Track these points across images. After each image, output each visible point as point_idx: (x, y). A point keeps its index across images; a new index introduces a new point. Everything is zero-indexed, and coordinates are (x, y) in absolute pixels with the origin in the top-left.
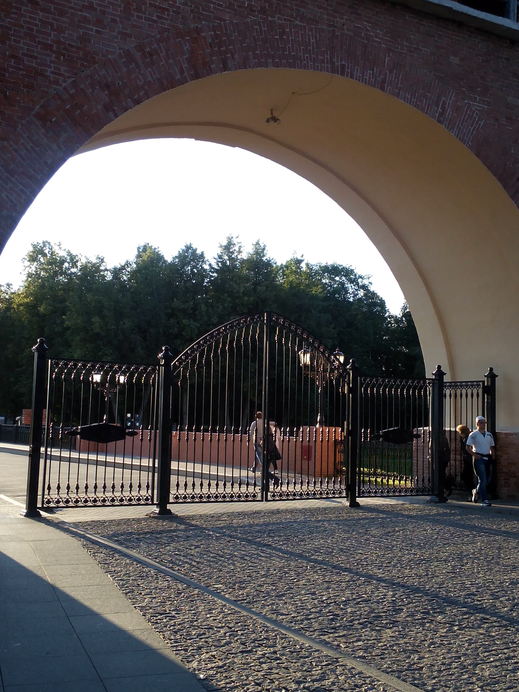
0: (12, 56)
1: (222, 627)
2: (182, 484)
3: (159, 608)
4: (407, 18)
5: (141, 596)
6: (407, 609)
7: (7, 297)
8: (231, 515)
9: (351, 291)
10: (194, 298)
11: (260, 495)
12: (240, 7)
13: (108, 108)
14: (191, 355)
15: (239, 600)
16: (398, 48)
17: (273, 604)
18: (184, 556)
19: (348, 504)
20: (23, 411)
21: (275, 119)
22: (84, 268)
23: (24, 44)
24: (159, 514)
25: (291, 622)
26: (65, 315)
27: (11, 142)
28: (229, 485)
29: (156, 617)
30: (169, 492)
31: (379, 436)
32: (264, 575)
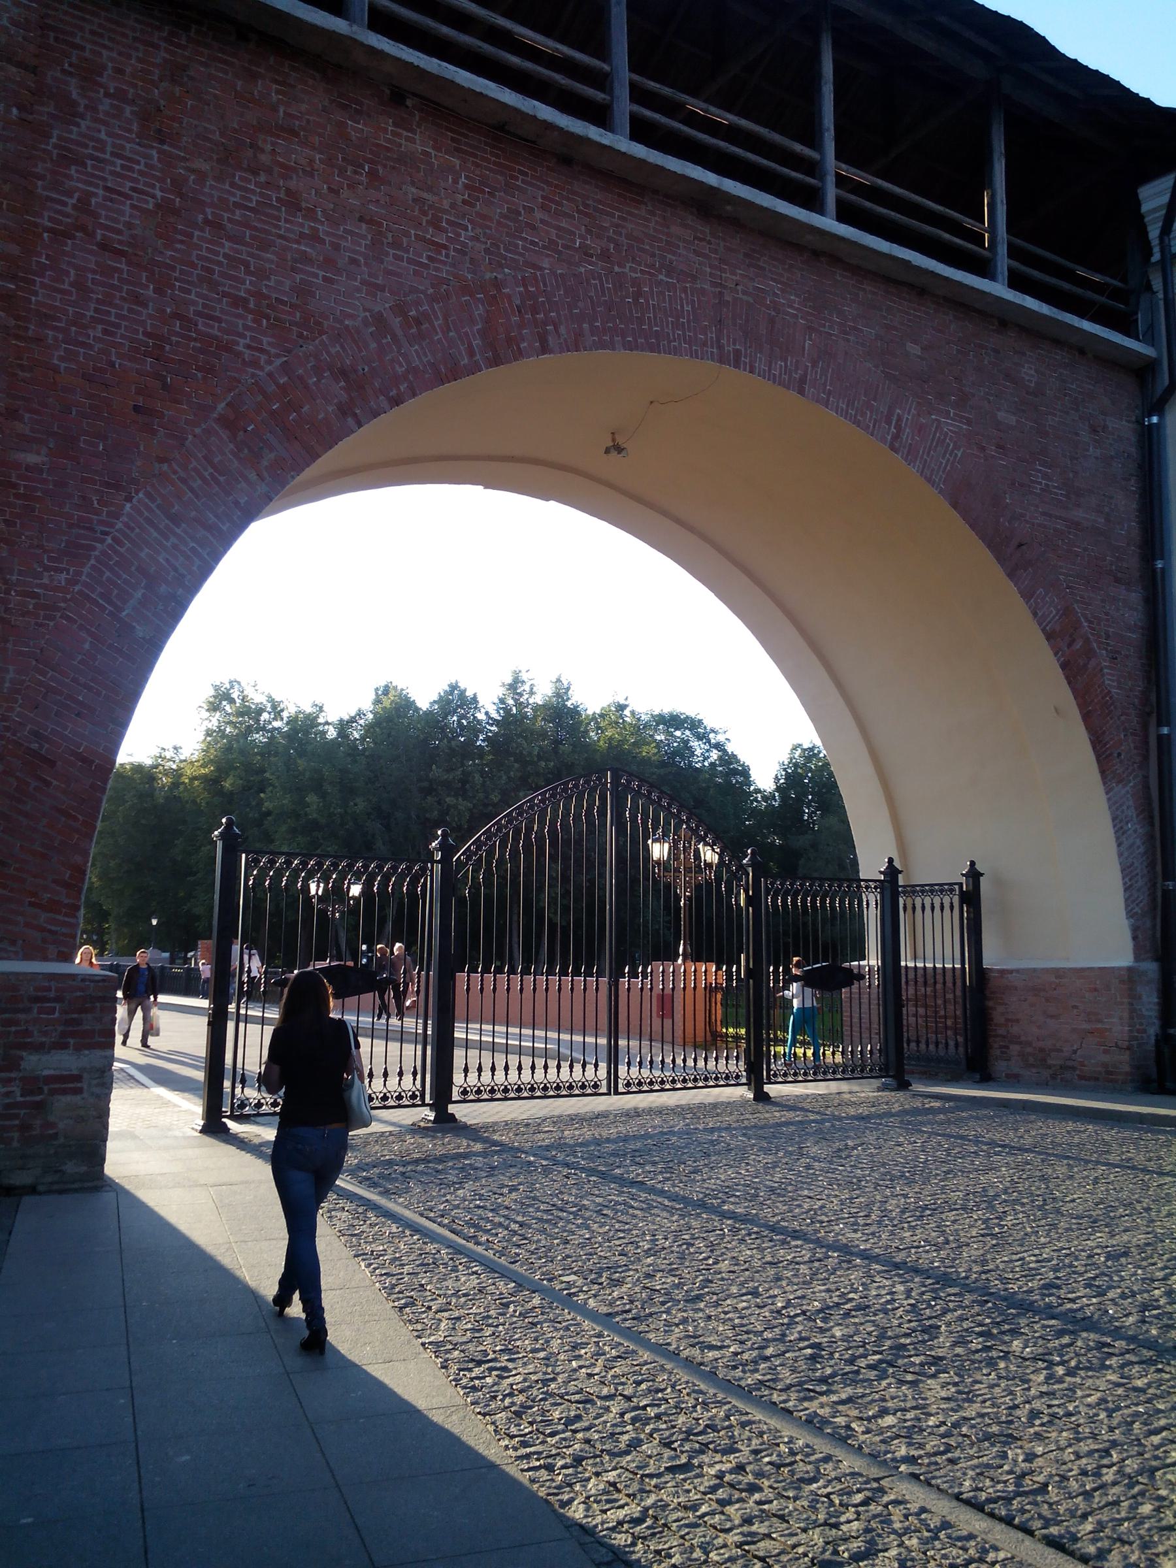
0: (176, 316)
2: (473, 1065)
5: (431, 1315)
6: (948, 1324)
7: (174, 767)
8: (559, 1121)
9: (698, 752)
10: (463, 765)
11: (604, 1083)
12: (566, 247)
13: (345, 410)
15: (617, 1313)
16: (824, 326)
17: (684, 1321)
18: (492, 1210)
19: (752, 1096)
21: (619, 449)
22: (292, 721)
23: (198, 295)
24: (434, 1122)
25: (735, 1367)
26: (264, 792)
27: (176, 467)
28: (565, 1066)
29: (470, 1370)
32: (650, 1249)
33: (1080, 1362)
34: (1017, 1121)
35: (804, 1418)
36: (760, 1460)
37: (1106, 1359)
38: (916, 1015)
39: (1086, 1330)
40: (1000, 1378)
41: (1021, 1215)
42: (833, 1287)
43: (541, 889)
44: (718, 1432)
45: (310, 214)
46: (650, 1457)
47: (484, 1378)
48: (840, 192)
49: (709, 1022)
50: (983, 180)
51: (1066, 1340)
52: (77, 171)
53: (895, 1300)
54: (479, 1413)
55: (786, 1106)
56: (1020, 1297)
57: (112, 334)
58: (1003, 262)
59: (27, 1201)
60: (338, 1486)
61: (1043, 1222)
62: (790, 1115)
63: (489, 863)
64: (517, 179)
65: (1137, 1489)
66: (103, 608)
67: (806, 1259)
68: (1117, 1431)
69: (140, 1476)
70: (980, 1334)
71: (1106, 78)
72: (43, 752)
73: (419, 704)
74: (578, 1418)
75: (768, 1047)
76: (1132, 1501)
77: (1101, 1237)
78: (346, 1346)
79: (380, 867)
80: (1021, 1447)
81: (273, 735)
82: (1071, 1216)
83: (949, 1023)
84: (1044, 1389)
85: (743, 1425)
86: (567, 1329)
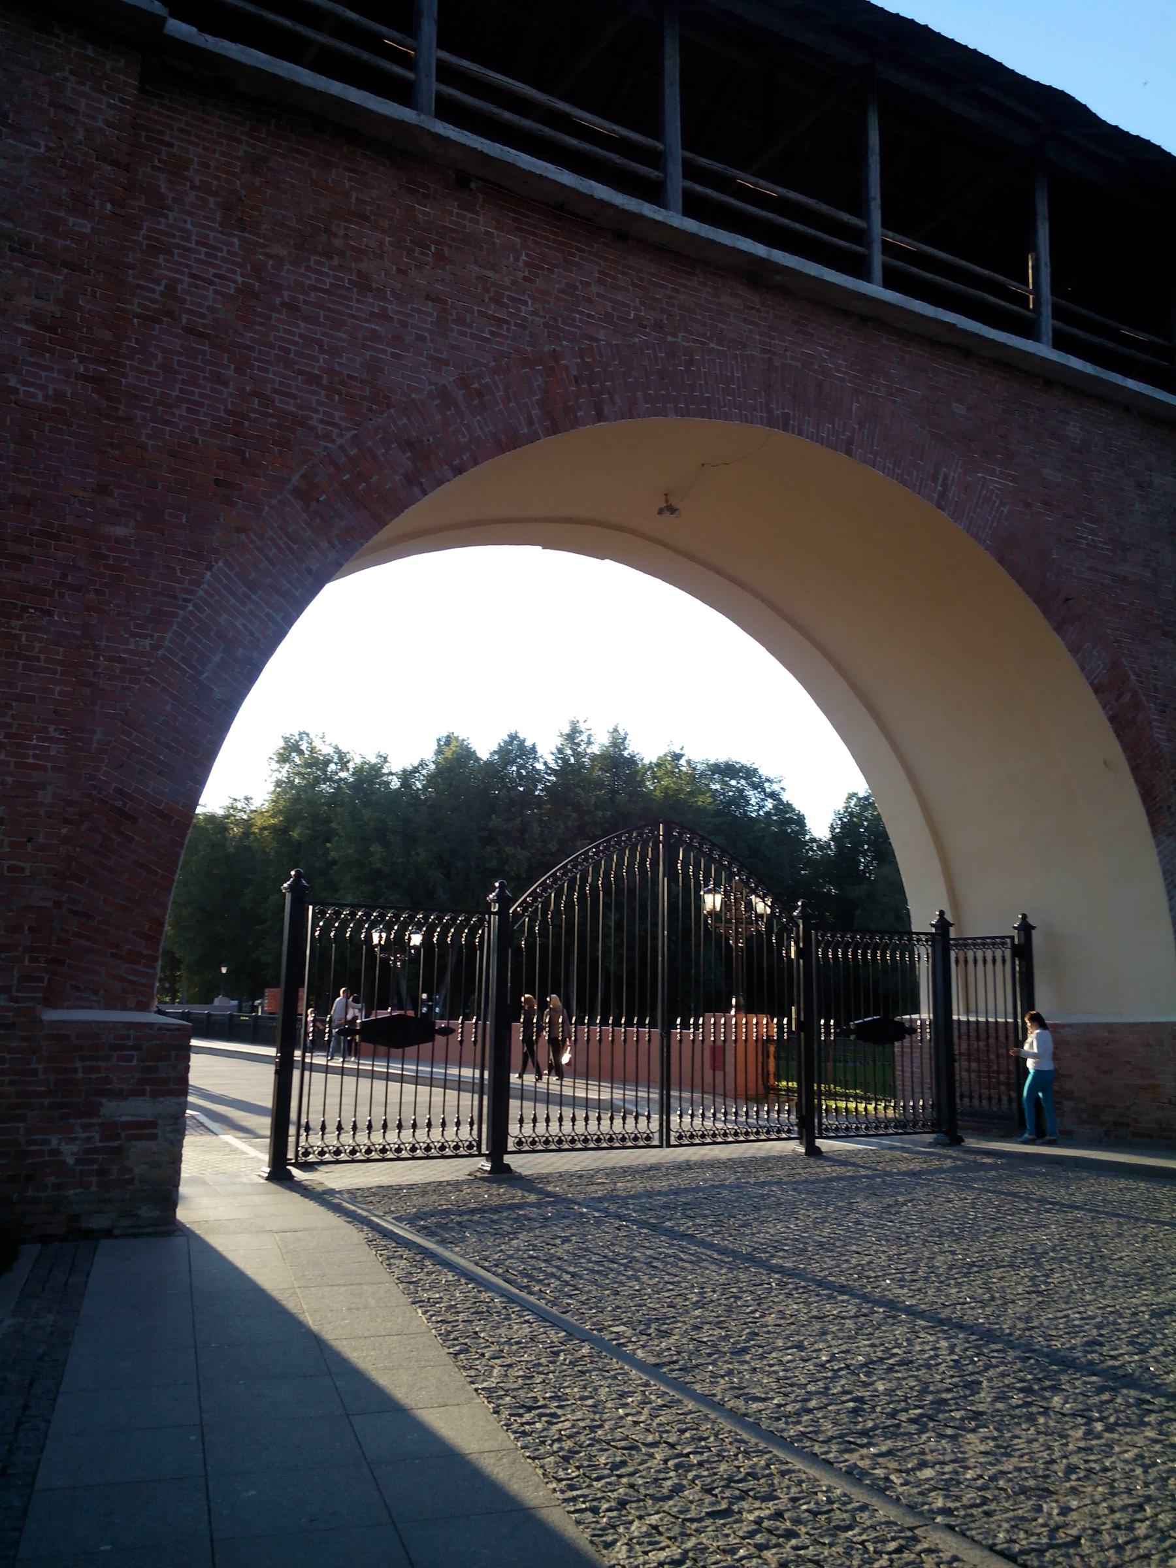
0: (255, 394)
1: (654, 1444)
3: (522, 1393)
4: (885, 342)
5: (484, 1361)
6: (990, 1380)
7: (245, 817)
8: (613, 1173)
9: (753, 801)
11: (657, 1135)
12: (621, 319)
13: (411, 480)
14: (541, 896)
15: (664, 1364)
17: (730, 1373)
18: (545, 1261)
19: (803, 1150)
20: (267, 990)
21: (672, 510)
22: (358, 771)
24: (490, 1172)
25: (778, 1419)
27: (253, 536)
28: (606, 1117)
29: (521, 1416)
30: (506, 1133)
31: (849, 1032)
32: (698, 1302)
33: (1118, 1418)
34: (1068, 1178)
35: (844, 1469)
36: (798, 1507)
37: (1145, 1416)
38: (969, 1070)
39: (1124, 1387)
40: (1039, 1433)
41: (1068, 1273)
42: (877, 1342)
43: (595, 939)
44: (758, 1479)
45: (380, 294)
46: (691, 1502)
47: (534, 1423)
48: (888, 259)
49: (765, 1075)
50: (1027, 244)
51: (1106, 1396)
52: (165, 260)
53: (937, 1356)
54: (529, 1457)
55: (837, 1161)
56: (1062, 1354)
57: (196, 412)
58: (1047, 323)
59: (105, 1243)
60: (393, 1523)
61: (1089, 1280)
62: (841, 1170)
63: (545, 914)
64: (574, 255)
65: (1168, 1543)
66: (183, 671)
67: (852, 1313)
68: (1152, 1487)
69: (209, 1510)
70: (1021, 1390)
71: (1147, 143)
72: (126, 809)
73: (479, 755)
74: (623, 1463)
75: (820, 1100)
76: (1162, 1554)
77: (1146, 1295)
78: (403, 1390)
79: (440, 918)
80: (1057, 1501)
81: (339, 787)
82: (1118, 1274)
83: (1002, 1078)
84: (1082, 1444)
85: (783, 1474)
86: (615, 1377)
